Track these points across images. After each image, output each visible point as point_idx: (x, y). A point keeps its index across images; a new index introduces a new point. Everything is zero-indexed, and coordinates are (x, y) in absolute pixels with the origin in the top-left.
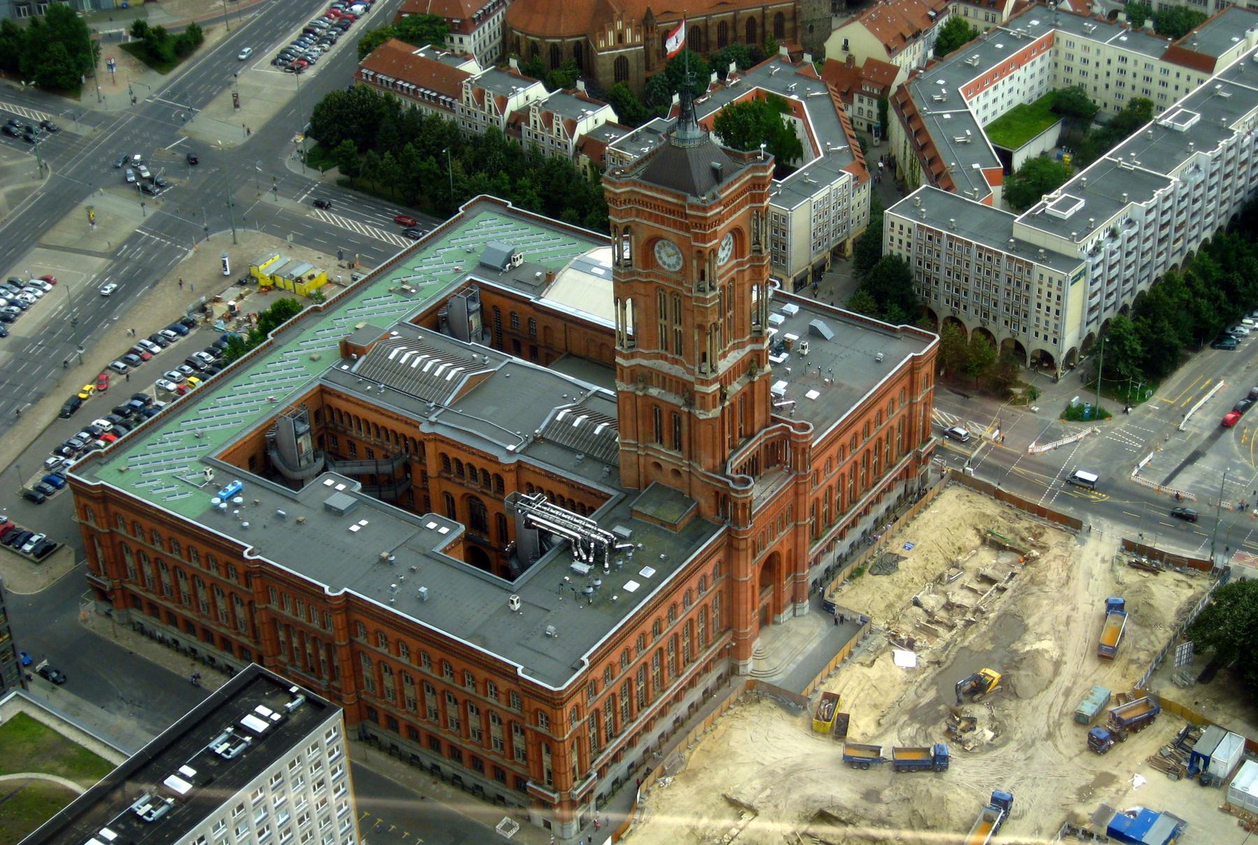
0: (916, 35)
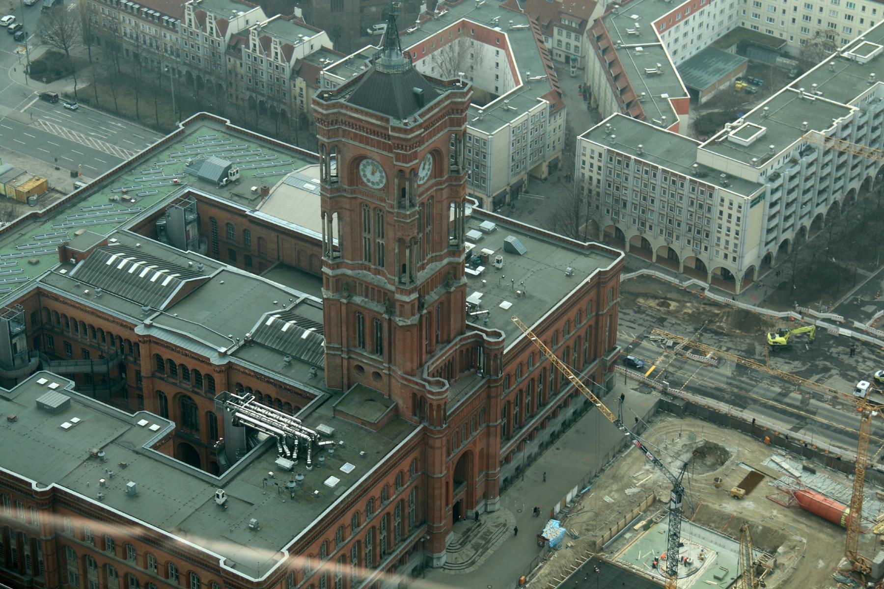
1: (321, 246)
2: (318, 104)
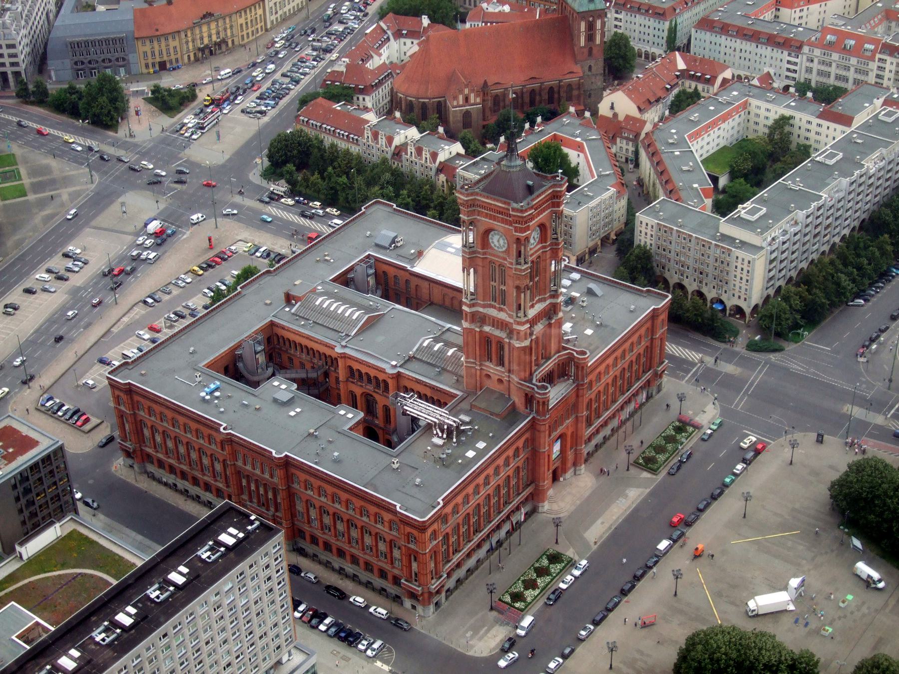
1: (462, 292)
2: (461, 193)
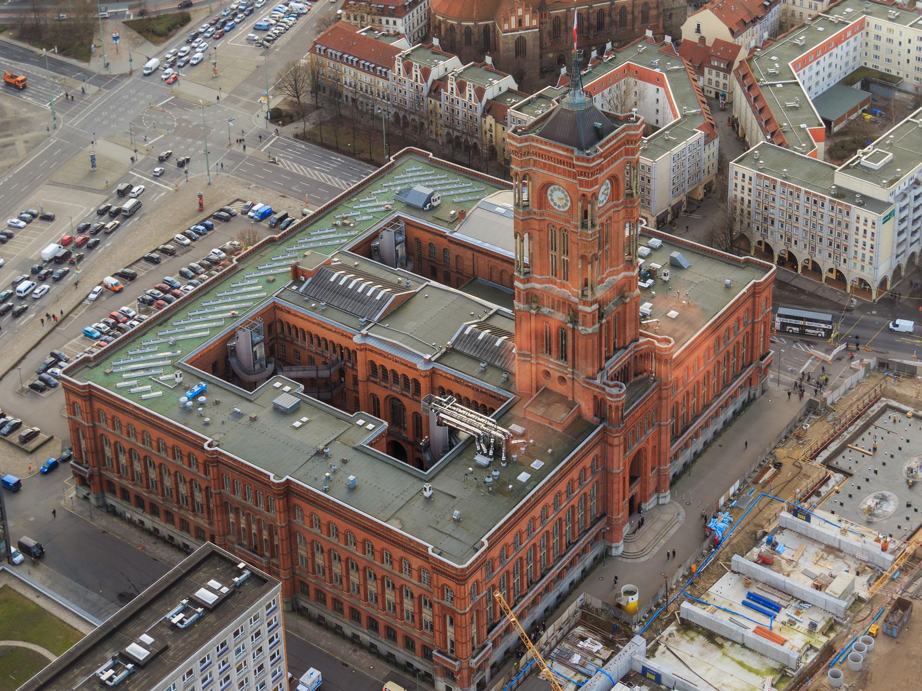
0: (754, 21)
1: (513, 264)
2: (513, 138)
